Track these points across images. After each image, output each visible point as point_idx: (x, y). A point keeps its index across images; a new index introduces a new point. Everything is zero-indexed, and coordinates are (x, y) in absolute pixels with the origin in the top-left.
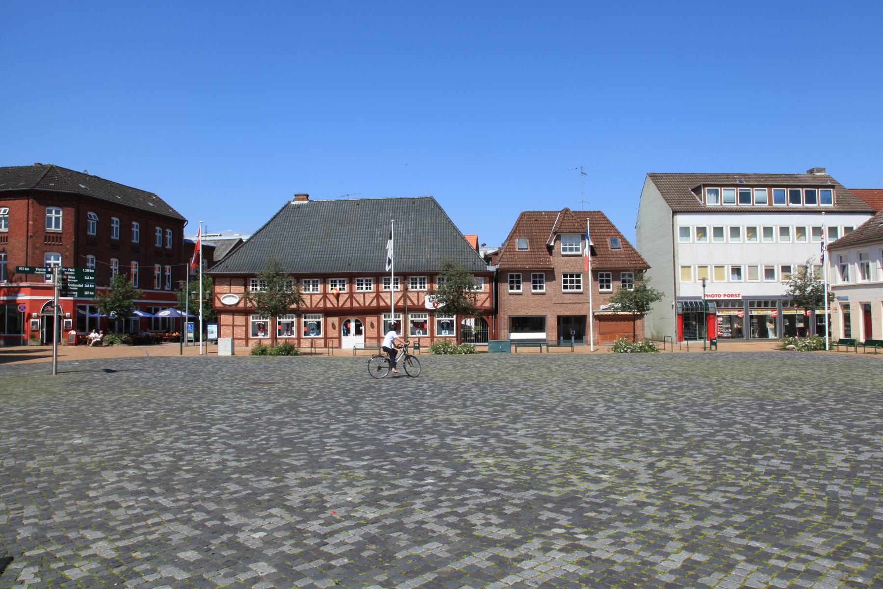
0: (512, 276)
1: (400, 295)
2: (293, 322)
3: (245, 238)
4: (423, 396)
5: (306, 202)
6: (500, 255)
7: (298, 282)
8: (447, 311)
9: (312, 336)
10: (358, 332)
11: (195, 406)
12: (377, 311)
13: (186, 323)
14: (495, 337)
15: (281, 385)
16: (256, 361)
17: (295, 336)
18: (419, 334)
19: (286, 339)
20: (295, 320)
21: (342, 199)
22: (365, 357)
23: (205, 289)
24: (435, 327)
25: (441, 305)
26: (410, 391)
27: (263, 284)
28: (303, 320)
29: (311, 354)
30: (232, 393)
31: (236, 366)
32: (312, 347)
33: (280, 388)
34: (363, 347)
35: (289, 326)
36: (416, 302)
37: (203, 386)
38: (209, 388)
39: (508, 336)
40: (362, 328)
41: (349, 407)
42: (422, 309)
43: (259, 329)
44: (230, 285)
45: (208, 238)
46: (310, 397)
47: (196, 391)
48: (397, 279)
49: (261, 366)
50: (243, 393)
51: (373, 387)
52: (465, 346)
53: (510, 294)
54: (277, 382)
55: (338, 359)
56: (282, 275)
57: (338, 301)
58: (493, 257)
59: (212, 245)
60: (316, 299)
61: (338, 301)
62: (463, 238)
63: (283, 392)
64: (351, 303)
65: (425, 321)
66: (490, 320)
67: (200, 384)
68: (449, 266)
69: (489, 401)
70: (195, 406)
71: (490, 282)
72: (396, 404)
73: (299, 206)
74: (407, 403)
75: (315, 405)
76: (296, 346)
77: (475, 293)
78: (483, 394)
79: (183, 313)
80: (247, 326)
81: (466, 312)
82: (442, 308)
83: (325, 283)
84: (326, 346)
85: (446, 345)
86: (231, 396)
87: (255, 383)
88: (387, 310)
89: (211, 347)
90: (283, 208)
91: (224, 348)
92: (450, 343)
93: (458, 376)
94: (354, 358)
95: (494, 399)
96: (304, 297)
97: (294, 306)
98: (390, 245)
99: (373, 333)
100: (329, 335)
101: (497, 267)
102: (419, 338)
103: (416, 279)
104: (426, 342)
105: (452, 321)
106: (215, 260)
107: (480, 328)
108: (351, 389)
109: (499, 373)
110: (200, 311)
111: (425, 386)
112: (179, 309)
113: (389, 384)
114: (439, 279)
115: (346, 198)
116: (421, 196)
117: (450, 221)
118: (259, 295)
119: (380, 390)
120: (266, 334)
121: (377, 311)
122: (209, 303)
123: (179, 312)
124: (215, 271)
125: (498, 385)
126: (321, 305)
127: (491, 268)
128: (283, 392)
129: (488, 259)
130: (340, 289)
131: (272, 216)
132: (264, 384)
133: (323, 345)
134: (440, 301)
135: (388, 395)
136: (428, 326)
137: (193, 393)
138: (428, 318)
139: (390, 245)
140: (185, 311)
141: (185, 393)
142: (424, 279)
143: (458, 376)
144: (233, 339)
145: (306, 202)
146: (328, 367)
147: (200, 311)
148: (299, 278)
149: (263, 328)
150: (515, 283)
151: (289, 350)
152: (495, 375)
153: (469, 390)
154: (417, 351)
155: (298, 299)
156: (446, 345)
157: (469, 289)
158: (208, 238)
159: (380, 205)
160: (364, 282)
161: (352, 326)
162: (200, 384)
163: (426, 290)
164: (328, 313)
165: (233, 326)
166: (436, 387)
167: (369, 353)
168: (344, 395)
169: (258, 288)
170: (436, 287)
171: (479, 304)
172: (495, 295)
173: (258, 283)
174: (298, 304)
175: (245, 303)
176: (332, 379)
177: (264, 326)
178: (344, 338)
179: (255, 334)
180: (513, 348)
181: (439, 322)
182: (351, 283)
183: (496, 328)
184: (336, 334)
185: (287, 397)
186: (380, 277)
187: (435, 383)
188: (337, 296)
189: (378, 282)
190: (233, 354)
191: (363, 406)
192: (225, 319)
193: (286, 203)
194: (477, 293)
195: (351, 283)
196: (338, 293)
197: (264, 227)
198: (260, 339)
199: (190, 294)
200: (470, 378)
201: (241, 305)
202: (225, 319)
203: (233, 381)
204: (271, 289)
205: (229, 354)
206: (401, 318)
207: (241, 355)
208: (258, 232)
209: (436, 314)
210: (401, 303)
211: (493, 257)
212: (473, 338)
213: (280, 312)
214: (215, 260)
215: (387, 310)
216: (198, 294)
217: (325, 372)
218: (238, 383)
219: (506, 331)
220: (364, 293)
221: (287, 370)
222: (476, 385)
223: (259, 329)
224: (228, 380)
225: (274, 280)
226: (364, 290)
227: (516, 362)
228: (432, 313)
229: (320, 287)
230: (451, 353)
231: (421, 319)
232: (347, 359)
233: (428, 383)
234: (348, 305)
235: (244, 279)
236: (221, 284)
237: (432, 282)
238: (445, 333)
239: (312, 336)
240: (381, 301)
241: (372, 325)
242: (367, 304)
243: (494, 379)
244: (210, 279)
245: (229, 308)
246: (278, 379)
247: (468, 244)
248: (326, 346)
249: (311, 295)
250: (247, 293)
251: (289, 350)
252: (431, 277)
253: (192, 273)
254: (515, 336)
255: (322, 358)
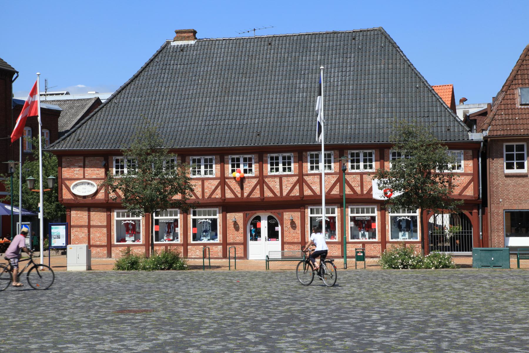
0: (510, 148)
1: (333, 179)
2: (176, 220)
3: (104, 97)
4: (372, 332)
5: (192, 42)
6: (490, 115)
7: (183, 161)
8: (406, 202)
9: (205, 240)
10: (273, 235)
11: (33, 346)
12: (300, 203)
13: (19, 223)
14: (484, 242)
15: (161, 314)
16: (123, 279)
17: (180, 240)
18: (364, 237)
19: (166, 245)
20: (179, 217)
21: (246, 36)
22: (283, 272)
23: (46, 174)
24: (389, 227)
25: (397, 194)
26: (352, 324)
27: (132, 165)
28: (191, 217)
29: (203, 267)
30: (90, 326)
31: (95, 286)
32: (204, 257)
33: (159, 319)
34: (279, 256)
35: (171, 226)
36: (358, 190)
37: (45, 317)
38: (54, 319)
39: (505, 242)
40: (279, 229)
41: (261, 347)
42: (367, 200)
43: (128, 230)
44: (84, 167)
45: (49, 98)
46: (204, 332)
47: (35, 324)
48: (329, 156)
49: (131, 286)
50: (105, 326)
51: (297, 317)
52: (435, 256)
53: (507, 176)
54: (155, 310)
55: (243, 275)
56: (161, 152)
57: (242, 188)
58: (479, 119)
59: (56, 107)
60: (211, 185)
61: (242, 188)
62: (431, 90)
63: (164, 324)
64: (262, 192)
65: (373, 218)
66: (474, 216)
67: (40, 314)
68: (410, 134)
69: (477, 342)
70: (33, 346)
71: (474, 157)
72: (331, 343)
73: (182, 49)
74: (349, 343)
75: (211, 343)
76: (182, 255)
77: (451, 175)
78: (468, 331)
79: (15, 210)
80: (109, 226)
81: (435, 203)
82: (398, 198)
83: (222, 162)
84: (225, 256)
85: (406, 254)
86: (87, 330)
87: (122, 311)
88: (315, 201)
89: (56, 259)
90: (160, 52)
91: (76, 260)
92: (412, 250)
93: (426, 302)
94: (267, 273)
95: (486, 340)
96: (192, 183)
97: (178, 197)
98: (320, 102)
99: (295, 235)
100: (230, 240)
101: (486, 133)
102: (364, 244)
103: (358, 155)
104: (374, 250)
105: (414, 218)
106: (60, 130)
107: (458, 228)
108: (264, 320)
109: (492, 300)
110: (40, 205)
111: (375, 317)
112: (8, 203)
113: (320, 313)
114: (394, 154)
115: (252, 35)
116: (365, 28)
117: (410, 65)
118: (127, 182)
119: (306, 321)
120: (137, 239)
121: (300, 203)
122: (53, 194)
123: (9, 208)
124: (62, 146)
125: (490, 317)
126: (218, 195)
127: (476, 136)
128: (164, 324)
129: (470, 121)
130: (245, 171)
131: (143, 64)
132: (135, 312)
133: (220, 255)
134: (396, 188)
135: (320, 330)
136: (377, 225)
137: (30, 327)
138: (376, 214)
139: (320, 102)
140: (17, 206)
141: (18, 328)
142: (370, 154)
143: (426, 302)
144: (89, 246)
145: (192, 42)
146: (229, 288)
147: (40, 205)
148: (184, 154)
149: (132, 229)
150: (516, 158)
151: (171, 262)
152: (485, 303)
153: (444, 324)
154: (360, 264)
155: (184, 186)
156: (406, 254)
157: (441, 168)
158: (49, 98)
159: (302, 42)
160: (281, 160)
161: (264, 225)
162: (40, 314)
163: (373, 170)
164: (227, 206)
165: (89, 227)
166: (392, 318)
167: (291, 265)
168: (254, 329)
169: (126, 170)
170: (389, 165)
171: (456, 192)
172: (482, 178)
173: (125, 163)
174: (183, 193)
175: (107, 194)
176: (236, 305)
177: (134, 226)
178: (252, 244)
179: (121, 239)
180: (513, 261)
181: (394, 219)
182: (261, 161)
183: (485, 229)
184: (240, 238)
185: (169, 331)
186: (304, 152)
187: (390, 312)
188: (241, 181)
189: (301, 160)
190: (89, 268)
191: (282, 345)
192: (77, 217)
193: (162, 43)
194: (453, 174)
195: (261, 161)
196: (243, 178)
197: (132, 81)
198: (129, 246)
199: (24, 181)
200: (445, 306)
201: (101, 196)
202: (77, 217)
203: (89, 309)
204: (144, 171)
205: (84, 268)
206: (337, 214)
207: (101, 269)
208: (123, 88)
209: (389, 207)
210: (336, 191)
211: (479, 119)
212: (448, 244)
213: (158, 206)
214: (60, 130)
215: (315, 201)
216: (36, 181)
217: (225, 294)
218: (98, 312)
219: (502, 234)
220: (281, 177)
221: (169, 291)
222: (456, 317)
223: (128, 230)
224: (82, 307)
225: (149, 158)
226: (281, 172)
227: (519, 282)
228: (382, 205)
229: (216, 169)
230: (414, 267)
231: (367, 215)
232: (256, 275)
233: (379, 313)
234: (257, 194)
235: (104, 158)
236: (70, 165)
237: (382, 158)
238: (403, 237)
239: (205, 240)
240: (305, 188)
241: (293, 224)
242: (285, 194)
243: (483, 310)
244: (54, 158)
245: (82, 201)
246: (155, 305)
247: (438, 99)
248: (225, 256)
249: (203, 180)
250: (108, 177)
251: (171, 262)
252: (381, 150)
253: (28, 150)
254: (515, 241)
255: (219, 274)
